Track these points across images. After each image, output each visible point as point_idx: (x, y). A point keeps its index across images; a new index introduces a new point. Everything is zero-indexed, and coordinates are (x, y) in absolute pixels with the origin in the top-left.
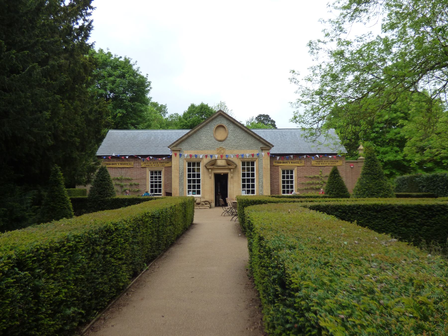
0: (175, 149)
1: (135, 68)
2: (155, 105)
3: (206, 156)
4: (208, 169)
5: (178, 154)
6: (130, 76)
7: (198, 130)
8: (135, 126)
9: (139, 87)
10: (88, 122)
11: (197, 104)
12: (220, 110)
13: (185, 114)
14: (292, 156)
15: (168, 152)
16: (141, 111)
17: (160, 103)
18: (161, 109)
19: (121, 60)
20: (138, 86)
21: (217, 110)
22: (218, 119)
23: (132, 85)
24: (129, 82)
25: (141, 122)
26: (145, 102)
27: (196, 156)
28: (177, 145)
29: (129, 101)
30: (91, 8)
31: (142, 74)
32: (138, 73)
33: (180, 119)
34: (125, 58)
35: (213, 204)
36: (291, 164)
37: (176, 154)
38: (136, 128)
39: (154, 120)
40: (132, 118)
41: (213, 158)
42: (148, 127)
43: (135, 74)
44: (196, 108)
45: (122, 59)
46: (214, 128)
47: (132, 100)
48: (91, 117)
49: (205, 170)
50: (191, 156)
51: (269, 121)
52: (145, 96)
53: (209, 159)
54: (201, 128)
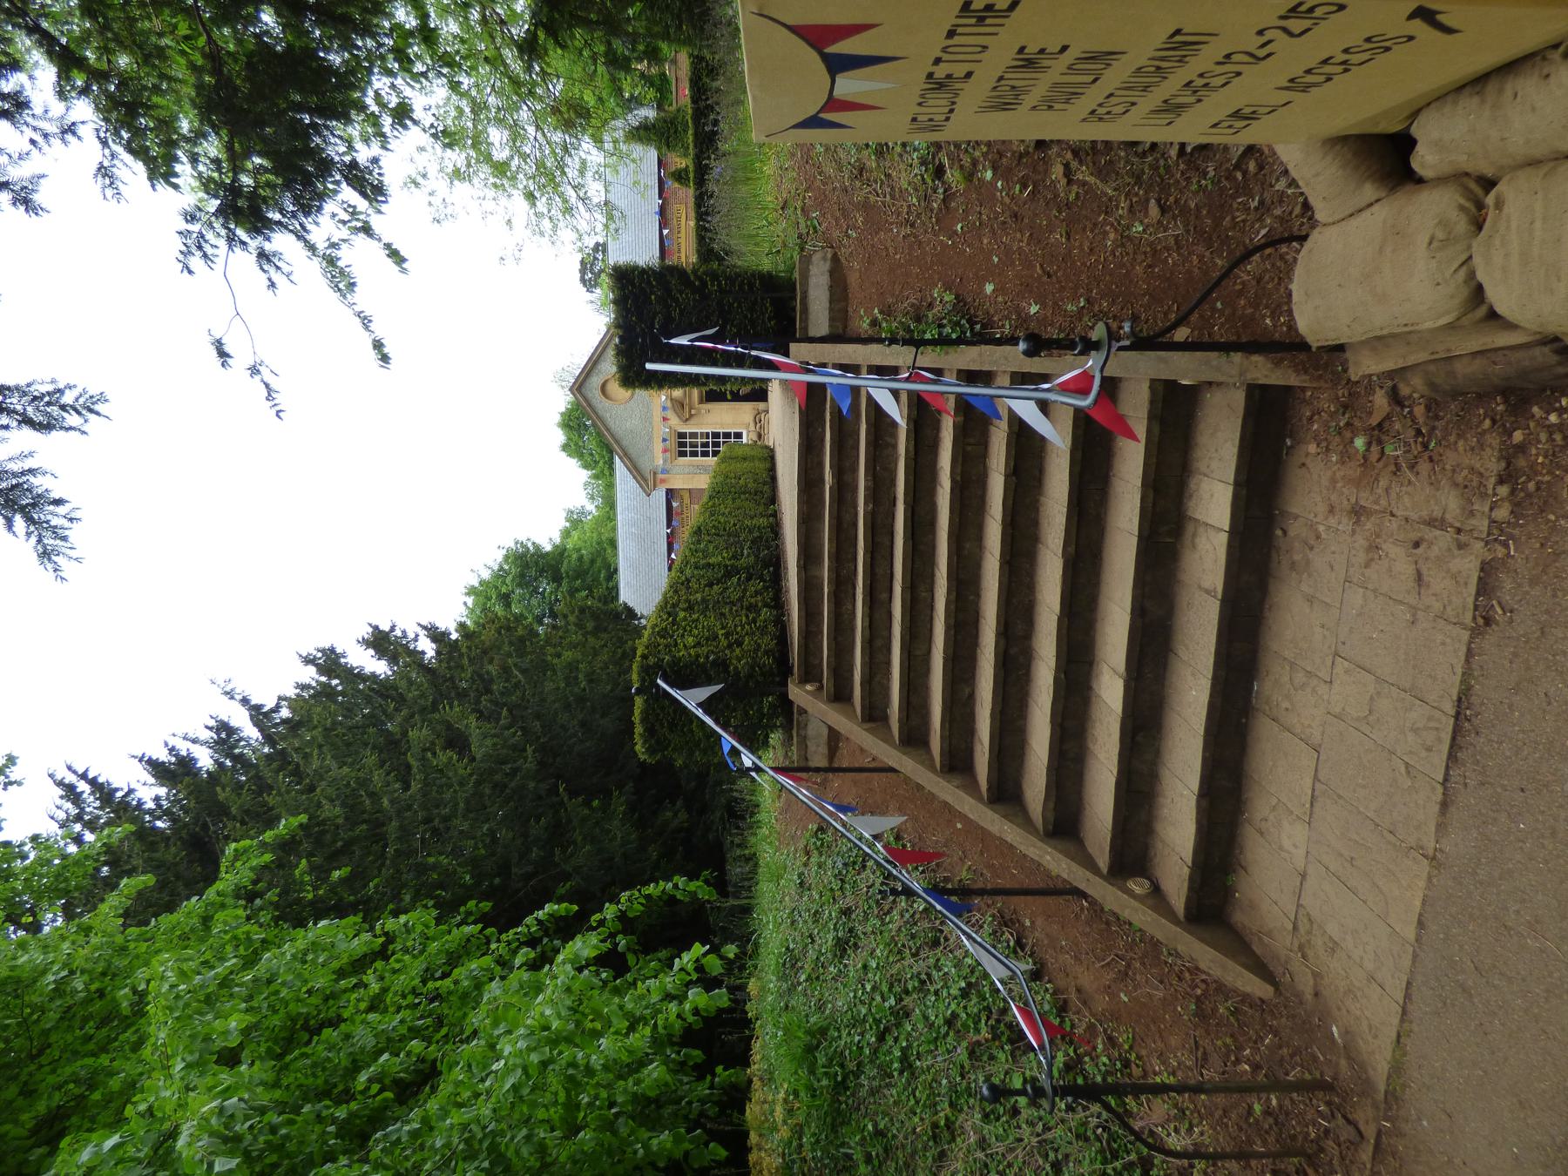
0: (651, 483)
1: (486, 575)
2: (566, 534)
3: (665, 419)
4: (691, 416)
5: (660, 476)
6: (504, 583)
7: (613, 436)
8: (612, 573)
9: (529, 566)
10: (597, 631)
11: (560, 437)
12: (571, 390)
13: (586, 466)
14: (665, 232)
15: (659, 496)
16: (580, 558)
17: (564, 524)
18: (575, 521)
19: (470, 604)
20: (526, 566)
21: (570, 398)
22: (590, 395)
23: (523, 580)
24: (520, 585)
25: (605, 559)
26: (560, 552)
27: (664, 440)
28: (646, 480)
29: (560, 585)
30: (393, 628)
31: (500, 559)
32: (496, 568)
33: (596, 477)
34: (468, 594)
35: (761, 405)
36: (683, 235)
37: (663, 481)
38: (616, 570)
39: (600, 534)
40: (596, 579)
41: (669, 404)
42: (613, 543)
43: (500, 575)
44: (569, 439)
45: (470, 601)
46: (607, 403)
47: (557, 578)
48: (590, 625)
49: (692, 421)
50: (665, 451)
51: (595, 258)
52: (547, 554)
53: (670, 414)
54: (608, 430)
